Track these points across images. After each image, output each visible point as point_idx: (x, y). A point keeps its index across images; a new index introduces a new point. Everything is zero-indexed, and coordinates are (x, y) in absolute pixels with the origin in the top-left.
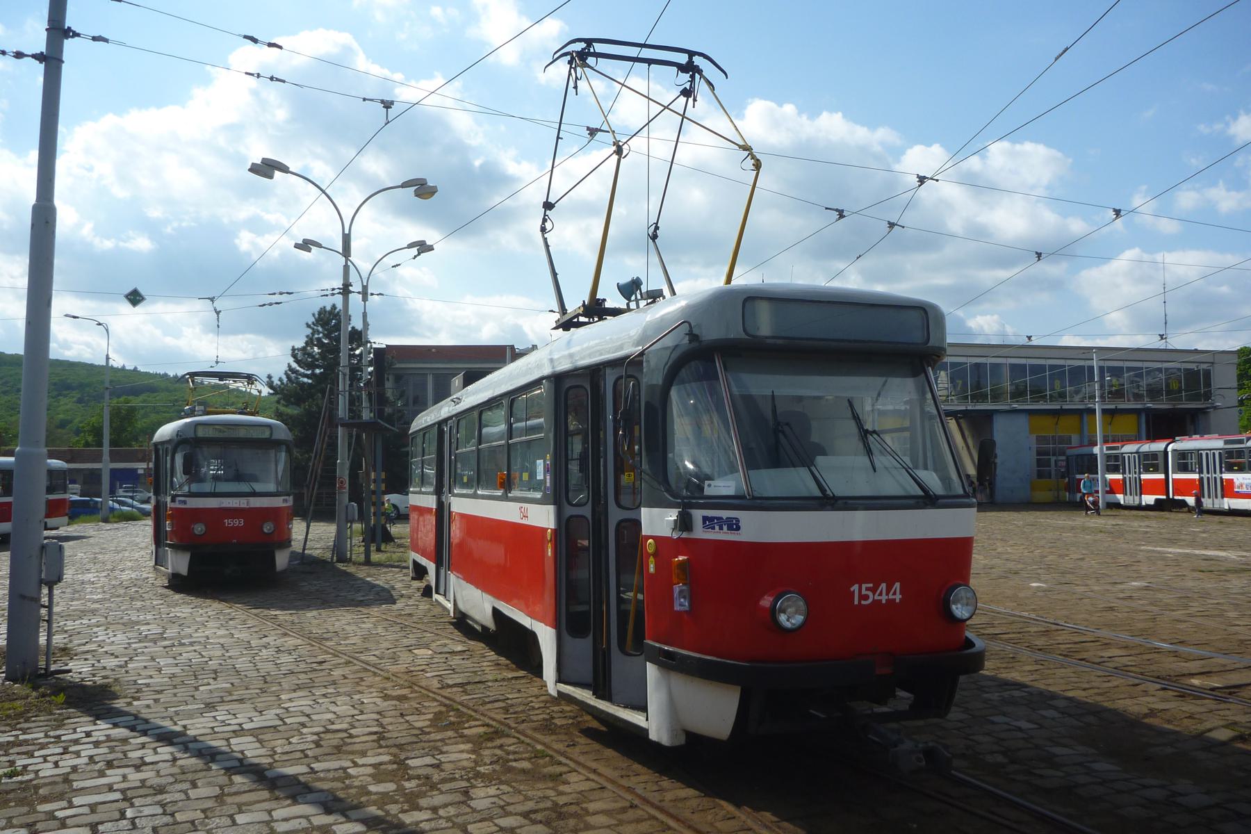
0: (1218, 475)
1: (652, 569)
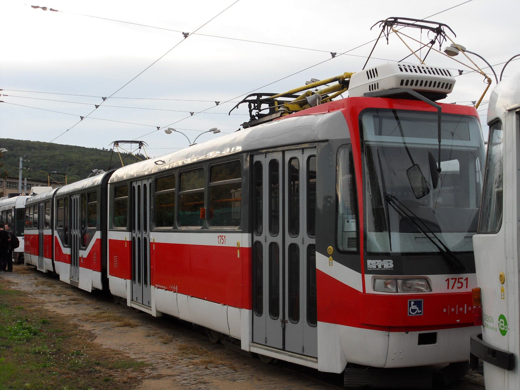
0: (266, 238)
1: (238, 256)
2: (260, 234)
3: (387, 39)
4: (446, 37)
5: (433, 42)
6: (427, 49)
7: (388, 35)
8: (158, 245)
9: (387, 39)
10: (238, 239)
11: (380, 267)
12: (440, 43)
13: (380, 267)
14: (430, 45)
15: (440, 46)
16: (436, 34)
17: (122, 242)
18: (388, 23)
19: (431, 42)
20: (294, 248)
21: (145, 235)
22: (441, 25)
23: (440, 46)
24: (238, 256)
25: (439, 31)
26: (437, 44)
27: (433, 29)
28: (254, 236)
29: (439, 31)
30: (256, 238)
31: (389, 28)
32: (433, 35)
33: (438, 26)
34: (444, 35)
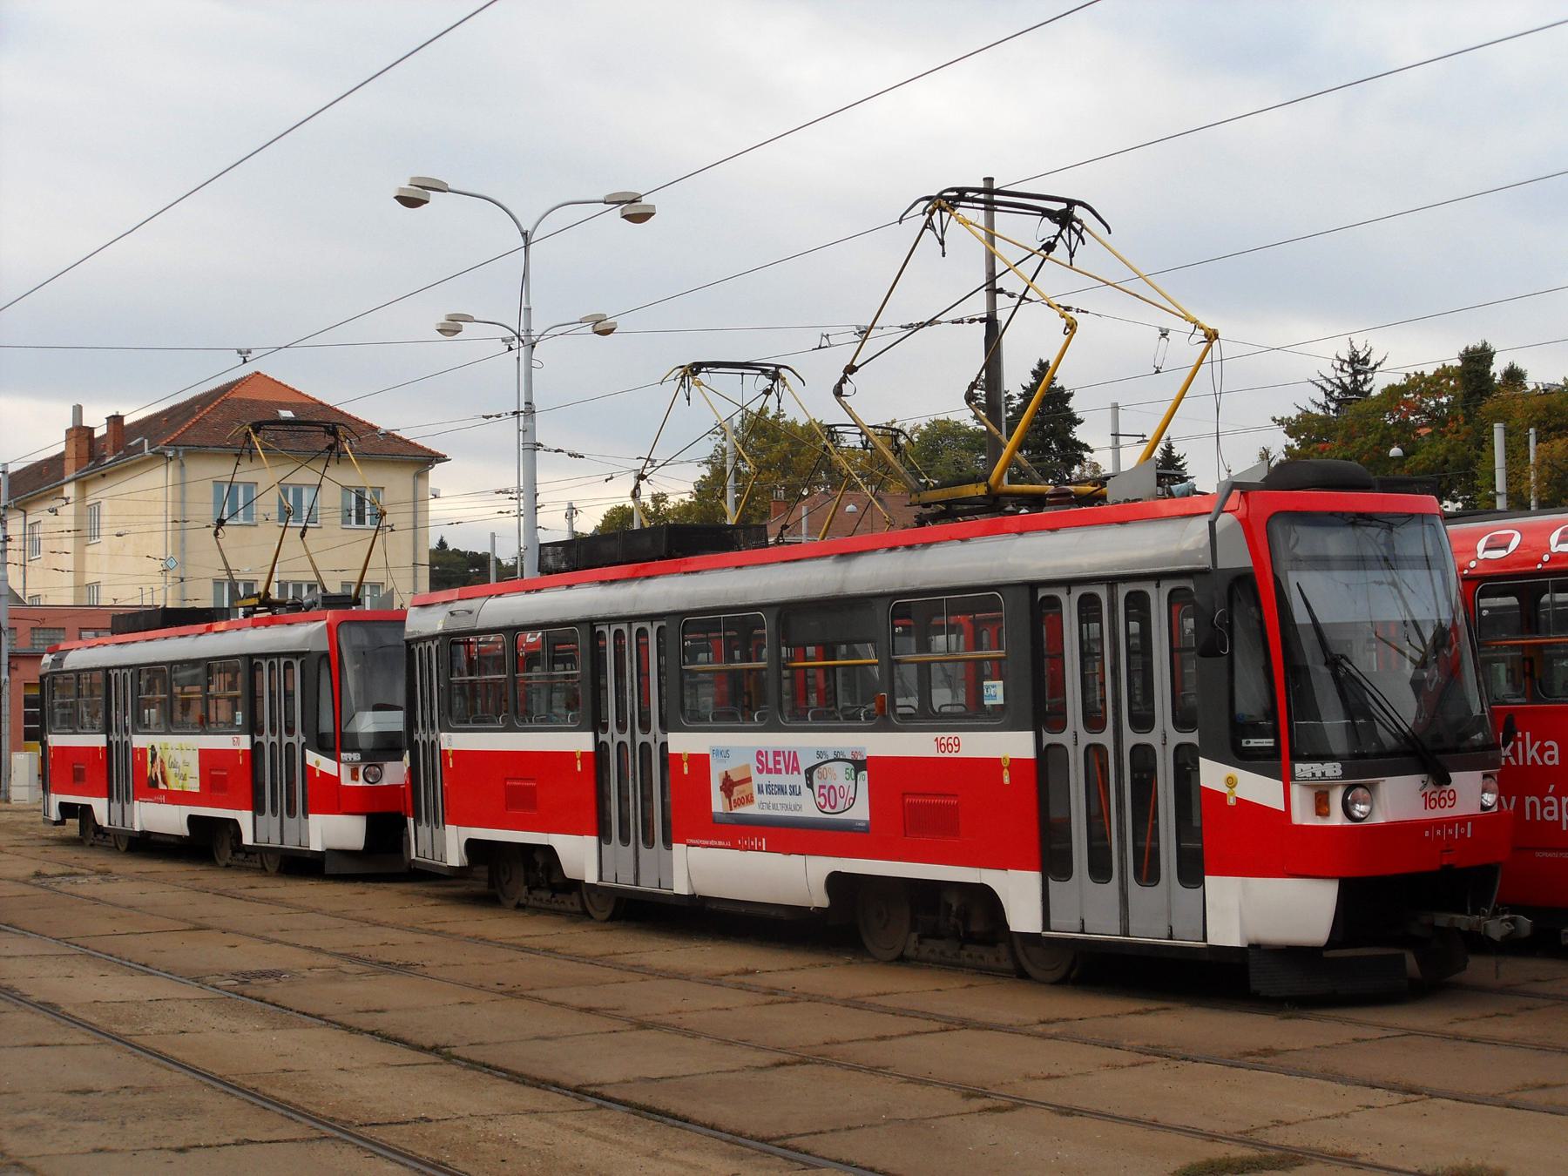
0: (653, 737)
1: (1006, 780)
2: (1060, 725)
3: (942, 243)
4: (1084, 233)
5: (1049, 247)
6: (1037, 259)
7: (943, 232)
8: (459, 755)
9: (942, 243)
10: (582, 742)
11: (1319, 774)
12: (1069, 247)
13: (1319, 774)
14: (1043, 252)
15: (1072, 255)
16: (1057, 228)
17: (569, 757)
18: (943, 204)
19: (1043, 247)
20: (1143, 755)
21: (125, 738)
22: (1071, 203)
23: (1072, 255)
24: (1006, 780)
25: (1065, 219)
26: (1061, 251)
27: (1046, 213)
28: (1045, 734)
29: (1065, 219)
30: (257, 738)
31: (946, 215)
32: (1050, 228)
33: (1064, 206)
34: (1078, 227)
